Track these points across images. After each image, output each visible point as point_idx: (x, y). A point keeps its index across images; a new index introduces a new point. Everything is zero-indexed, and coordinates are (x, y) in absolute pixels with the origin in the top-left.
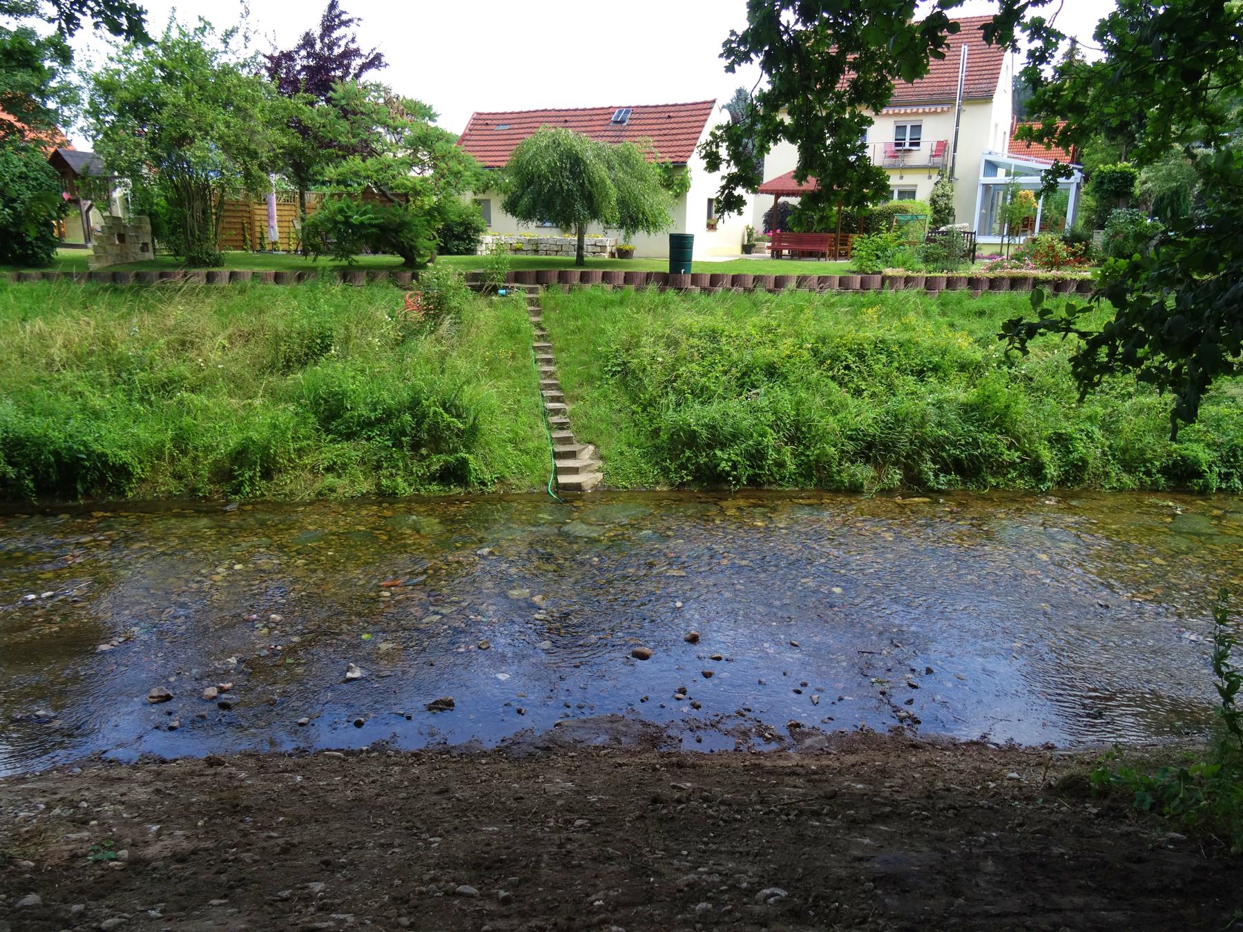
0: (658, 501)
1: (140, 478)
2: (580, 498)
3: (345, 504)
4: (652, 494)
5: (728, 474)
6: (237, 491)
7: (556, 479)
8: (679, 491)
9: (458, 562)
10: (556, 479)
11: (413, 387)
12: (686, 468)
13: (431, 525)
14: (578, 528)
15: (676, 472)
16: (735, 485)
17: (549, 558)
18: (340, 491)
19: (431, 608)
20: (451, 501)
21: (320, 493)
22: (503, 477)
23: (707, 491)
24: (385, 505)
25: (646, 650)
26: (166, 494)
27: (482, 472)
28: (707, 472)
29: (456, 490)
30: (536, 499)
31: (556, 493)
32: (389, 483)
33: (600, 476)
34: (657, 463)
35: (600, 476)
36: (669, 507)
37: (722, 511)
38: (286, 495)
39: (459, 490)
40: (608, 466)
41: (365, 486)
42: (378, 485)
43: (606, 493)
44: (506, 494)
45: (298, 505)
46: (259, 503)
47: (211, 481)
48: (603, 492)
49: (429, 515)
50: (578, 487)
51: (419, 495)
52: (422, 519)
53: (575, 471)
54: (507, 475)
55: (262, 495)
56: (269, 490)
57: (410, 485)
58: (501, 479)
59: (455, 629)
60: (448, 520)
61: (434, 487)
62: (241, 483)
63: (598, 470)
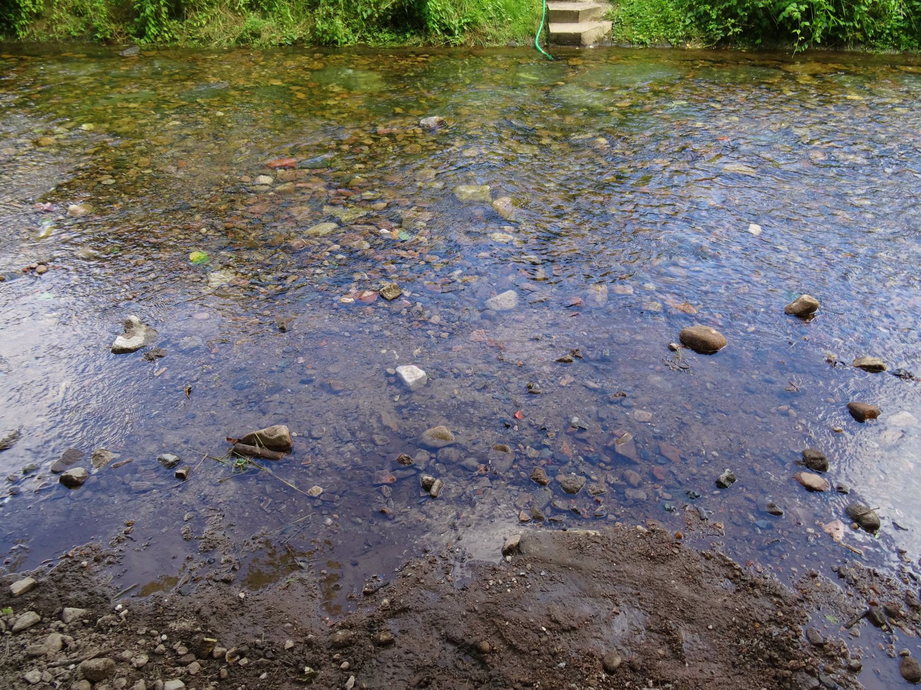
0: (689, 60)
1: (31, 13)
2: (577, 55)
3: (267, 54)
4: (678, 53)
5: (795, 24)
6: (141, 34)
7: (546, 28)
8: (718, 49)
9: (390, 135)
10: (546, 28)
11: (839, 483)
12: (735, 16)
13: (369, 81)
14: (573, 93)
15: (718, 20)
16: (801, 43)
17: (528, 136)
18: (265, 35)
19: (327, 209)
20: (403, 54)
21: (241, 39)
22: (475, 22)
23: (760, 51)
24: (317, 55)
25: (713, 334)
26: (64, 36)
27: (449, 16)
28: (765, 23)
29: (413, 40)
30: (517, 55)
31: (546, 47)
32: (326, 27)
33: (608, 25)
34: (691, 8)
35: (608, 25)
36: (707, 71)
37: (792, 78)
38: (201, 40)
39: (417, 39)
40: (620, 12)
41: (298, 32)
42: (313, 30)
43: (614, 49)
44: (479, 47)
45: (211, 52)
46: (164, 49)
47: (111, 20)
48: (610, 49)
49: (371, 69)
50: (577, 39)
51: (366, 46)
52: (360, 74)
53: (573, 17)
54: (481, 20)
55: (173, 39)
56: (180, 32)
57: (354, 31)
58: (472, 26)
59: (351, 252)
60: (395, 77)
61: (385, 36)
62: (145, 22)
63: (605, 18)
